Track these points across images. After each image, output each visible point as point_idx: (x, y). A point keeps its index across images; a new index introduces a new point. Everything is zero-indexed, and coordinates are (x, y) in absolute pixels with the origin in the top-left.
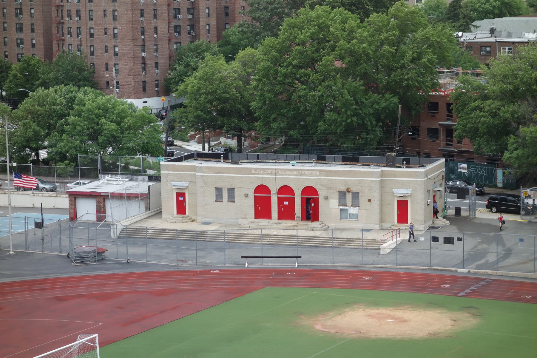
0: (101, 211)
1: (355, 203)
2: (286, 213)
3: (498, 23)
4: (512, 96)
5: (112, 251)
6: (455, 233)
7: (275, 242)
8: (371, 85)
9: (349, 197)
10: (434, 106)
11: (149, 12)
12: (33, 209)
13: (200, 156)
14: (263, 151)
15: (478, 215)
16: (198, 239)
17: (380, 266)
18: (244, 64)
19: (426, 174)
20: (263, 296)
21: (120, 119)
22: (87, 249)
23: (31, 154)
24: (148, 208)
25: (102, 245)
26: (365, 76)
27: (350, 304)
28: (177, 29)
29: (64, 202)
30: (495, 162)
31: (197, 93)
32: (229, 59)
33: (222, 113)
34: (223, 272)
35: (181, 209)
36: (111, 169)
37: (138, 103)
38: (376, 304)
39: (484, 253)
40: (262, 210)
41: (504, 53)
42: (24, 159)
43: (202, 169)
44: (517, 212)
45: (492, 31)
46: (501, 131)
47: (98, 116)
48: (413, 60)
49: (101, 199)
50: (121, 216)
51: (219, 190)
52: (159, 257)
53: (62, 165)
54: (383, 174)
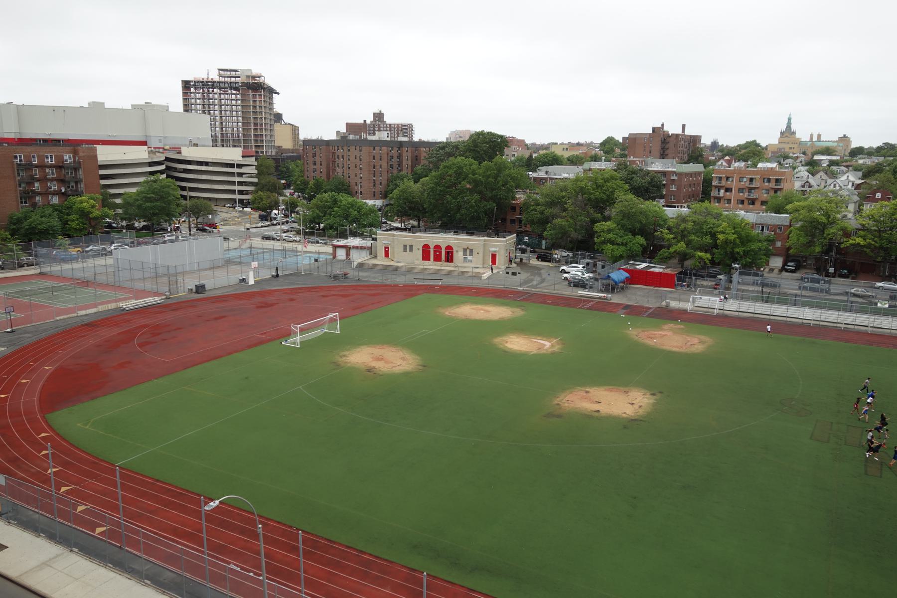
0: (348, 254)
1: (471, 254)
2: (438, 258)
3: (550, 168)
4: (551, 204)
5: (351, 274)
6: (518, 270)
7: (431, 272)
8: (484, 198)
9: (468, 251)
10: (513, 208)
11: (377, 157)
12: (316, 252)
13: (398, 229)
14: (431, 228)
15: (531, 262)
16: (393, 269)
17: (480, 285)
18: (585, 171)
19: (506, 241)
20: (422, 297)
21: (359, 209)
22: (338, 272)
23: (249, 264)
24: (371, 254)
25: (347, 271)
26: (480, 193)
27: (464, 303)
28: (392, 166)
29: (330, 250)
30: (541, 237)
31: (399, 198)
32: (416, 182)
33: (411, 208)
34: (404, 286)
35: (387, 255)
36: (354, 234)
37: (370, 203)
38: (476, 303)
39: (532, 280)
40: (426, 257)
41: (548, 184)
42: (313, 228)
43: (397, 236)
44: (550, 261)
45: (547, 172)
46: (544, 222)
47: (349, 208)
48: (503, 186)
49: (348, 249)
50: (358, 258)
51: (405, 246)
52: (374, 278)
53: (330, 231)
54: (485, 241)
